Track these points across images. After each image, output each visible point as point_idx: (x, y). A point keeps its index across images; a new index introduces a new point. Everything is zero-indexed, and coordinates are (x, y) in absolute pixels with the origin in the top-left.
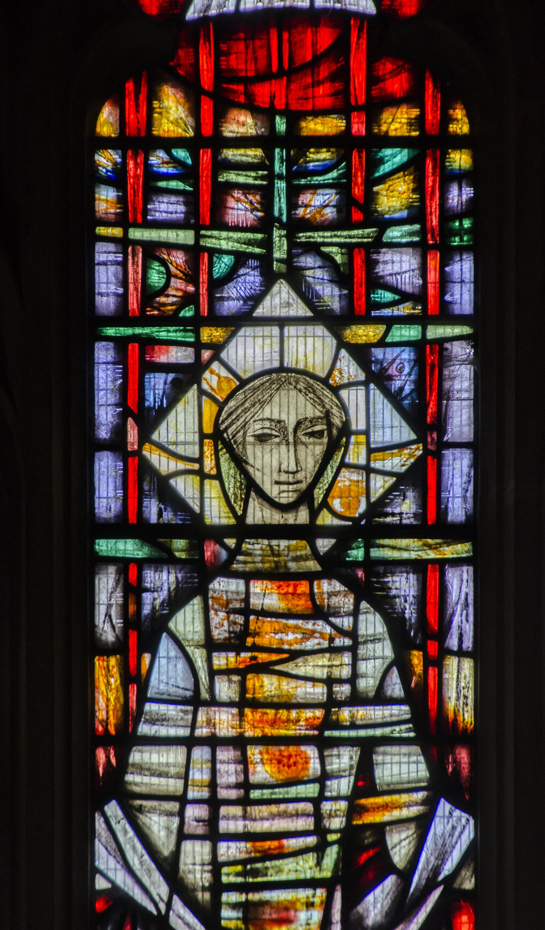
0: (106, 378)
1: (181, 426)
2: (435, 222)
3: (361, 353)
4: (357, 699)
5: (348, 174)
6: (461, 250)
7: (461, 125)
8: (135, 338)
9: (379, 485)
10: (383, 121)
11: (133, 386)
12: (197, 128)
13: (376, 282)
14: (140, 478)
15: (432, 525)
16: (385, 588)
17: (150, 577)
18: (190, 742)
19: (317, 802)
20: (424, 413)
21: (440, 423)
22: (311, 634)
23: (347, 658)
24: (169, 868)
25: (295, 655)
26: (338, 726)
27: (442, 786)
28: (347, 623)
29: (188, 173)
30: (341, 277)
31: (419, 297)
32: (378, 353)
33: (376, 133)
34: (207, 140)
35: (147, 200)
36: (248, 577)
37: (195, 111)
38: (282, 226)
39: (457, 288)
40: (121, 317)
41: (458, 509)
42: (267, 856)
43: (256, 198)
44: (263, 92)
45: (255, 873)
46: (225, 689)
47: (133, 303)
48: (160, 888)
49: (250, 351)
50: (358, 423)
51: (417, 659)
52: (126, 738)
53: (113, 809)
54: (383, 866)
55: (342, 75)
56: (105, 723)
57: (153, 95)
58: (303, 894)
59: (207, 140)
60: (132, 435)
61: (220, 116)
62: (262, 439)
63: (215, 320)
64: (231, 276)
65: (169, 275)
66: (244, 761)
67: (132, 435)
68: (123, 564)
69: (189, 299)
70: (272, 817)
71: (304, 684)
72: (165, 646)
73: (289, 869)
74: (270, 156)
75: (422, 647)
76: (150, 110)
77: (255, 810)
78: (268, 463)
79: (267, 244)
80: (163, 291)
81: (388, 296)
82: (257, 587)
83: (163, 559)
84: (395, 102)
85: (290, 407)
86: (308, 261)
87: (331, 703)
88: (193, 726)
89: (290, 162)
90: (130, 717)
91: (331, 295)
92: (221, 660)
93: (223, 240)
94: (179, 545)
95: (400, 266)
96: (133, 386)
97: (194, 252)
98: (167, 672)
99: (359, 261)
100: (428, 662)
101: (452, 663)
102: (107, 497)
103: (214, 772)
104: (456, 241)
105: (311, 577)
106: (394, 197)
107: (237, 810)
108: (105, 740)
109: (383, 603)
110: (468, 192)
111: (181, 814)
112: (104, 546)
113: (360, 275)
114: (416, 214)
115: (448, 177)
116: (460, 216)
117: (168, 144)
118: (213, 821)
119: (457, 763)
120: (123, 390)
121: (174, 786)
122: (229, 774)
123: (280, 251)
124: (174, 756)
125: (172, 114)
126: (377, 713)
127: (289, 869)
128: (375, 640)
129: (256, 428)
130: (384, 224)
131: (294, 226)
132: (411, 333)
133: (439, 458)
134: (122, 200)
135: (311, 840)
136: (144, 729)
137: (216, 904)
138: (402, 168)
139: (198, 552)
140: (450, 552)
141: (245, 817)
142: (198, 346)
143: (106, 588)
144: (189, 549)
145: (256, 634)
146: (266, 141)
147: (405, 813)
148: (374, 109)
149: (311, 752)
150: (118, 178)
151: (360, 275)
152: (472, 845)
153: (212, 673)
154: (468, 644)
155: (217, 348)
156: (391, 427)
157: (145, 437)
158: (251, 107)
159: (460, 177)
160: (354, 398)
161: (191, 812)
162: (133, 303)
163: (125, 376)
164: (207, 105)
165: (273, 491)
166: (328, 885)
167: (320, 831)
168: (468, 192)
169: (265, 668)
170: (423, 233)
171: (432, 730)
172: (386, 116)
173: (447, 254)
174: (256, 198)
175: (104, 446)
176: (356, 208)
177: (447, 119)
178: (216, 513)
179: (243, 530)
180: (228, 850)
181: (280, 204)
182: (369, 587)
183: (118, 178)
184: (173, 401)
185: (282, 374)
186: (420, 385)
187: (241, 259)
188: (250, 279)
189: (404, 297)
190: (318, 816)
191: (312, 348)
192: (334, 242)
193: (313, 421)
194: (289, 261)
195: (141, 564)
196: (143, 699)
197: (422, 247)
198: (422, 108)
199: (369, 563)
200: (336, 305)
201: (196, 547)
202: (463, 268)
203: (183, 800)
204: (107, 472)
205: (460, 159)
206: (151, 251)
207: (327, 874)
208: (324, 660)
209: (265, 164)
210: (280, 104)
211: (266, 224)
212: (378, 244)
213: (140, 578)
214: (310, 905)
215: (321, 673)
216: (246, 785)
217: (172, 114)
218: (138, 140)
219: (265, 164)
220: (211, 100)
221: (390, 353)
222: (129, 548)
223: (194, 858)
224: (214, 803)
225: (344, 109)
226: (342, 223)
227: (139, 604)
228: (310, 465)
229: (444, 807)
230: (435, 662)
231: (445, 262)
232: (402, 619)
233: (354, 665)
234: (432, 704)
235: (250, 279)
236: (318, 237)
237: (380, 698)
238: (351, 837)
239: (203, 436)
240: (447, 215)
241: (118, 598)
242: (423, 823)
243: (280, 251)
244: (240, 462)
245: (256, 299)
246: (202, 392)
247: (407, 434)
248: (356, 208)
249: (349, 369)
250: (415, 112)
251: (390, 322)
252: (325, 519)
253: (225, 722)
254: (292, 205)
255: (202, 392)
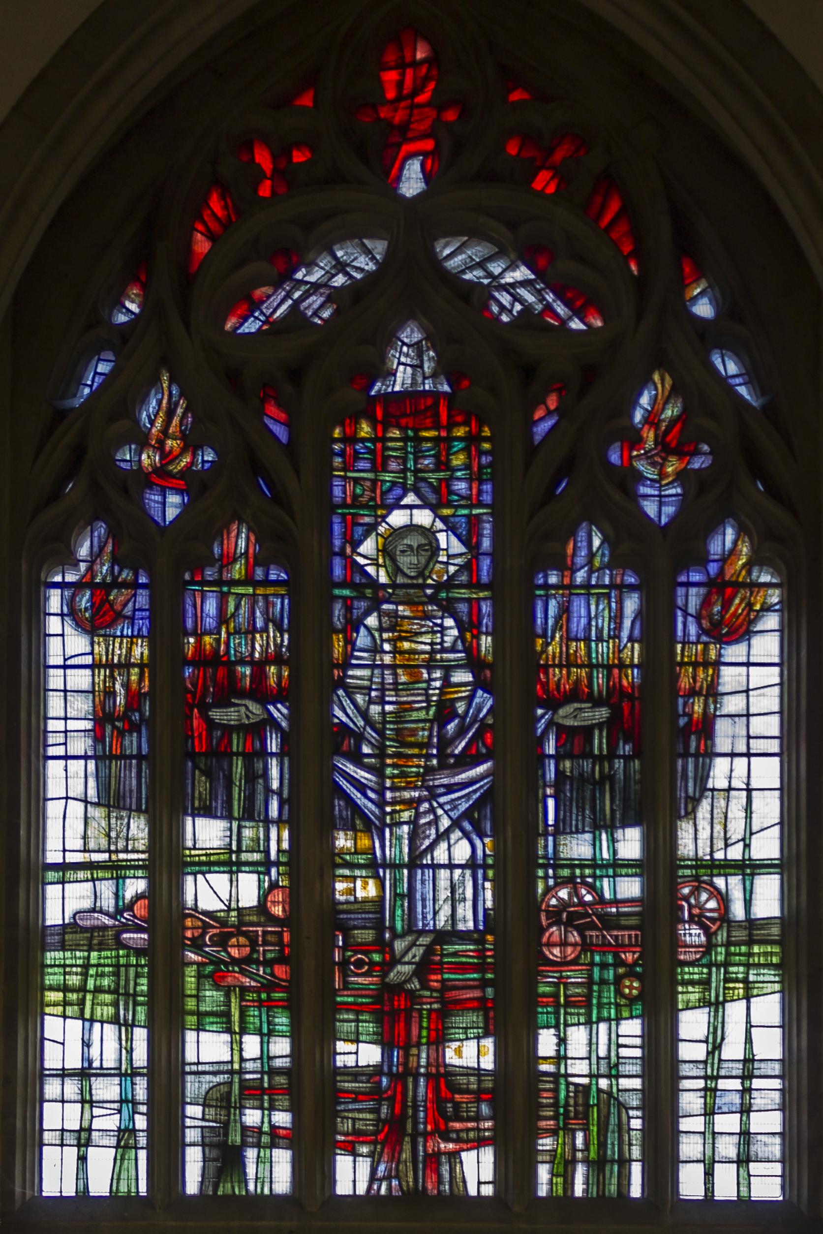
0: (337, 529)
1: (368, 546)
2: (476, 469)
3: (444, 519)
4: (444, 650)
5: (439, 453)
6: (487, 480)
7: (487, 432)
8: (350, 514)
9: (452, 569)
10: (68, 630)
11: (349, 532)
12: (376, 434)
13: (452, 492)
14: (353, 566)
15: (474, 584)
16: (455, 608)
17: (356, 603)
18: (372, 667)
19: (427, 690)
20: (470, 541)
21: (479, 544)
22: (423, 626)
23: (439, 635)
24: (364, 714)
25: (421, 634)
26: (436, 661)
27: (478, 684)
28: (439, 621)
29: (370, 451)
30: (436, 490)
31: (469, 498)
32: (452, 519)
33: (714, 302)
34: (380, 439)
35: (355, 461)
36: (397, 604)
37: (374, 428)
38: (411, 471)
39: (485, 495)
40: (344, 505)
41: (485, 578)
42: (406, 710)
43: (400, 461)
44: (403, 421)
45: (401, 717)
46: (387, 647)
47: (349, 501)
48: (361, 723)
49: (398, 518)
50: (443, 545)
51: (468, 635)
52: (346, 665)
53: (341, 692)
54: (454, 715)
55: (437, 415)
56: (338, 659)
57: (357, 423)
58: (421, 725)
59: (380, 439)
60: (348, 550)
61: (385, 430)
62: (403, 552)
63: (383, 506)
64: (390, 490)
65: (364, 490)
66: (395, 675)
67: (348, 550)
68: (345, 598)
69: (373, 499)
70: (408, 696)
71: (423, 644)
72: (362, 630)
73: (415, 715)
74: (406, 445)
75: (470, 631)
76: (356, 428)
77: (401, 693)
78: (406, 561)
79: (405, 478)
80: (362, 496)
81: (456, 498)
82: (400, 608)
83: (363, 597)
84: (458, 425)
85: (413, 541)
86: (422, 484)
87: (433, 652)
88: (374, 660)
89: (414, 447)
90: (348, 657)
91: (432, 498)
92: (385, 636)
93: (388, 477)
94: (368, 592)
95: (461, 486)
96: (349, 532)
97: (374, 482)
98: (362, 639)
99: (443, 485)
100: (473, 636)
101: (483, 637)
102: (338, 572)
103: (383, 678)
104: (485, 477)
105: (424, 604)
106: (458, 460)
107: (393, 693)
108: (337, 666)
109: (454, 616)
110: (490, 458)
111: (369, 695)
112: (337, 592)
113: (444, 490)
114: (467, 467)
115: (481, 453)
116: (486, 467)
117: (363, 440)
118: (383, 696)
119: (485, 676)
120: (345, 533)
121: (366, 683)
122: (389, 679)
123: (411, 481)
124: (366, 673)
125: (365, 429)
126: (451, 656)
127: (415, 715)
128: (451, 628)
129: (401, 548)
130: (454, 470)
131: (416, 471)
132: (465, 512)
133: (477, 560)
134: (344, 462)
135: (424, 705)
136: (354, 662)
137: (385, 729)
138: (462, 450)
139: (374, 595)
140: (481, 595)
141: (397, 695)
142: (376, 516)
143: (338, 609)
144: (373, 593)
145: (401, 626)
146: (405, 439)
147: (464, 694)
148: (450, 427)
149: (424, 671)
150: (342, 454)
151: (444, 490)
152: (492, 706)
153: (383, 641)
154: (490, 629)
155: (384, 517)
156: (457, 547)
157: (354, 551)
158: (399, 427)
159: (487, 453)
160: (442, 537)
161: (373, 694)
162: (349, 501)
163: (346, 527)
164: (380, 427)
165: (407, 571)
166: (431, 721)
167: (428, 701)
168: (490, 458)
169: (406, 639)
170: (470, 474)
171: (473, 662)
172: (455, 430)
173: (481, 482)
174: (400, 461)
175: (336, 554)
176: (442, 464)
177: (481, 431)
178: (383, 579)
179: (394, 585)
180: (388, 708)
181: (411, 464)
182: (448, 609)
183: (342, 454)
184: (365, 538)
185: (411, 528)
186: (469, 532)
187: (394, 484)
188: (398, 491)
189: (462, 498)
190: (428, 696)
191: (424, 517)
192: (433, 477)
193: (425, 545)
194: (414, 485)
195: (352, 599)
196: (353, 650)
197: (469, 480)
198: (470, 426)
199: (448, 599)
200: (434, 502)
201: (375, 593)
202: (487, 487)
203: (370, 689)
204: (338, 563)
205: (486, 446)
206: (357, 481)
207: (431, 717)
208: (430, 636)
209: (404, 448)
210: (410, 425)
211: (405, 471)
212: (452, 478)
213: (352, 605)
214: (423, 729)
215: (429, 641)
216: (396, 683)
217: (365, 429)
218: (350, 439)
219: (404, 448)
220: (381, 425)
221: (457, 519)
222: (346, 592)
223: (375, 709)
224: (382, 690)
225: (436, 426)
226: (437, 470)
227: (351, 613)
228: (423, 561)
229: (480, 693)
230: (477, 637)
231: (480, 484)
232: (462, 621)
233: (442, 638)
234: (475, 651)
235: (398, 491)
236: (426, 475)
237: (453, 650)
238: (440, 704)
239: (378, 550)
240: (481, 467)
241: (343, 612)
242: (471, 698)
243: (411, 481)
244: (394, 560)
245: (401, 498)
246: (378, 534)
247: (463, 550)
248: (442, 464)
249: (439, 525)
250: (467, 429)
251: (457, 507)
252: (430, 581)
253: (387, 659)
254: (416, 463)
255: (378, 534)
